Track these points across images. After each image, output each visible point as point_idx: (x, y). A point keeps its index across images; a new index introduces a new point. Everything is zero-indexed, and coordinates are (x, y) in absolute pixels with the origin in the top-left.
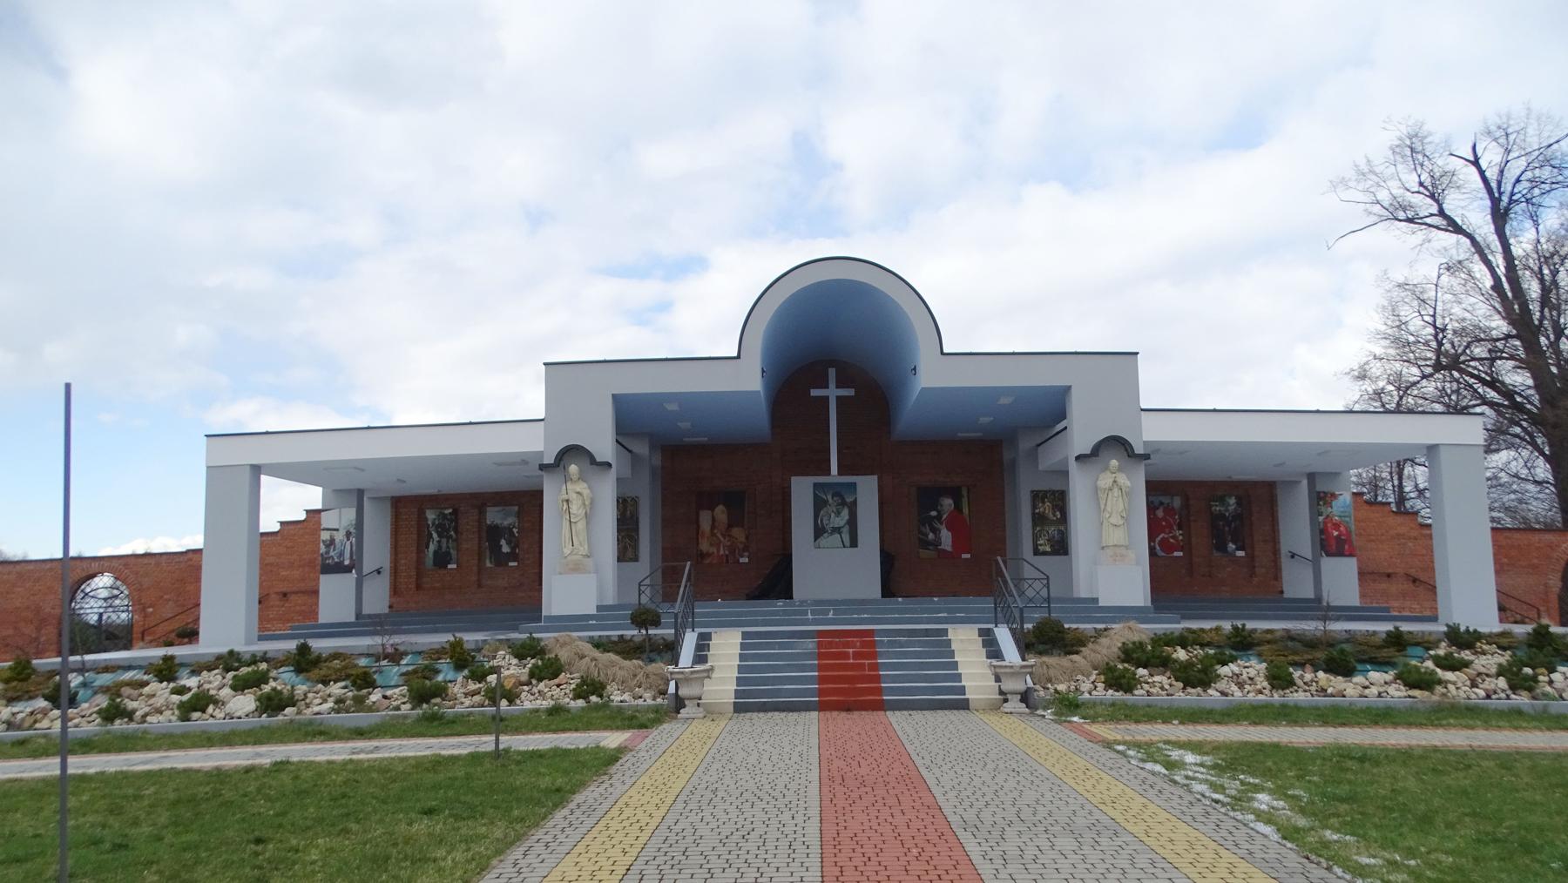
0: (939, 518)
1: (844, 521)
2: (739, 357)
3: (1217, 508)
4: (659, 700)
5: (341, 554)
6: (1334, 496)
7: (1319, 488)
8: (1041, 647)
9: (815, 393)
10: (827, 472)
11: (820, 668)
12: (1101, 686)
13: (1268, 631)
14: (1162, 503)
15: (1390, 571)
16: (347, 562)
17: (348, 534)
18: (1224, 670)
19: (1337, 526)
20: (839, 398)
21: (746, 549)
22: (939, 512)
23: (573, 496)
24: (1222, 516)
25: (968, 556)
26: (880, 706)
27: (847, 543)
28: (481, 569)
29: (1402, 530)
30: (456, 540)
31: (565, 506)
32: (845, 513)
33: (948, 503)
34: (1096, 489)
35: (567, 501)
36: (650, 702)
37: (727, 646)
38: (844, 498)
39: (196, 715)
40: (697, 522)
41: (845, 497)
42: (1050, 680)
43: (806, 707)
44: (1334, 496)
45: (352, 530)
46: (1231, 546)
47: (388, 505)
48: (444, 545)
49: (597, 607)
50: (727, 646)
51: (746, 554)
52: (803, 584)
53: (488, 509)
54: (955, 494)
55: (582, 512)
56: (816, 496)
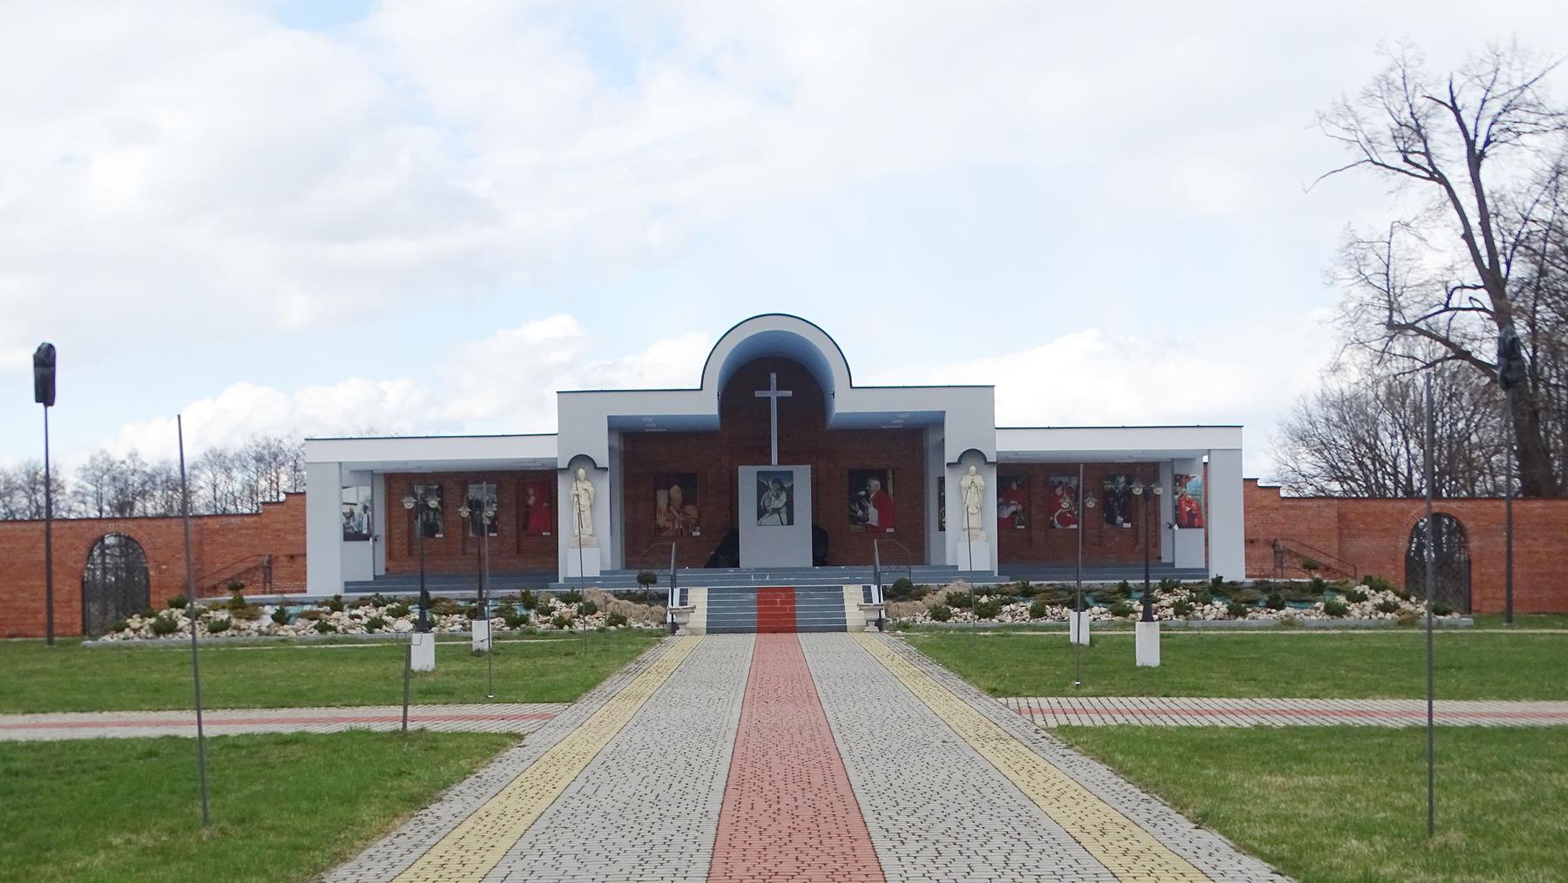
0: (867, 496)
1: (783, 503)
2: (701, 389)
3: (1109, 486)
4: (661, 627)
5: (360, 525)
6: (1188, 478)
7: (1177, 471)
8: (901, 597)
9: (758, 394)
10: (769, 463)
11: (759, 610)
12: (929, 618)
13: (1050, 585)
14: (1061, 483)
15: (1254, 538)
16: (365, 532)
17: (365, 508)
18: (1006, 608)
19: (1189, 503)
20: (779, 399)
21: (698, 523)
22: (867, 491)
23: (581, 492)
24: (1112, 493)
25: (892, 530)
26: (794, 630)
27: (785, 522)
28: (465, 539)
29: (1265, 502)
30: (442, 513)
31: (576, 499)
32: (784, 497)
33: (875, 484)
34: (960, 488)
35: (578, 495)
36: (655, 627)
37: (699, 597)
38: (783, 483)
39: (377, 630)
40: (655, 500)
41: (784, 482)
42: (899, 615)
43: (750, 631)
44: (1188, 478)
45: (368, 505)
46: (1120, 519)
47: (383, 479)
48: (432, 517)
49: (346, 584)
50: (699, 597)
51: (698, 528)
52: (747, 557)
53: (470, 486)
54: (881, 475)
55: (588, 504)
56: (759, 484)
